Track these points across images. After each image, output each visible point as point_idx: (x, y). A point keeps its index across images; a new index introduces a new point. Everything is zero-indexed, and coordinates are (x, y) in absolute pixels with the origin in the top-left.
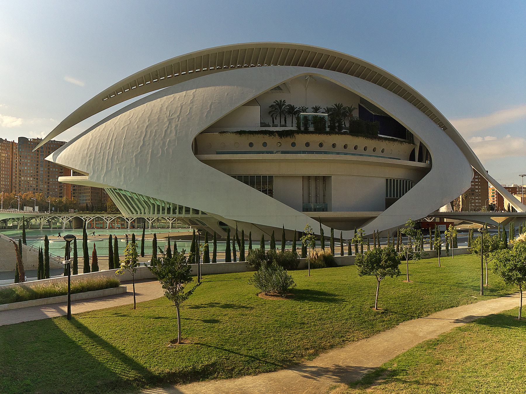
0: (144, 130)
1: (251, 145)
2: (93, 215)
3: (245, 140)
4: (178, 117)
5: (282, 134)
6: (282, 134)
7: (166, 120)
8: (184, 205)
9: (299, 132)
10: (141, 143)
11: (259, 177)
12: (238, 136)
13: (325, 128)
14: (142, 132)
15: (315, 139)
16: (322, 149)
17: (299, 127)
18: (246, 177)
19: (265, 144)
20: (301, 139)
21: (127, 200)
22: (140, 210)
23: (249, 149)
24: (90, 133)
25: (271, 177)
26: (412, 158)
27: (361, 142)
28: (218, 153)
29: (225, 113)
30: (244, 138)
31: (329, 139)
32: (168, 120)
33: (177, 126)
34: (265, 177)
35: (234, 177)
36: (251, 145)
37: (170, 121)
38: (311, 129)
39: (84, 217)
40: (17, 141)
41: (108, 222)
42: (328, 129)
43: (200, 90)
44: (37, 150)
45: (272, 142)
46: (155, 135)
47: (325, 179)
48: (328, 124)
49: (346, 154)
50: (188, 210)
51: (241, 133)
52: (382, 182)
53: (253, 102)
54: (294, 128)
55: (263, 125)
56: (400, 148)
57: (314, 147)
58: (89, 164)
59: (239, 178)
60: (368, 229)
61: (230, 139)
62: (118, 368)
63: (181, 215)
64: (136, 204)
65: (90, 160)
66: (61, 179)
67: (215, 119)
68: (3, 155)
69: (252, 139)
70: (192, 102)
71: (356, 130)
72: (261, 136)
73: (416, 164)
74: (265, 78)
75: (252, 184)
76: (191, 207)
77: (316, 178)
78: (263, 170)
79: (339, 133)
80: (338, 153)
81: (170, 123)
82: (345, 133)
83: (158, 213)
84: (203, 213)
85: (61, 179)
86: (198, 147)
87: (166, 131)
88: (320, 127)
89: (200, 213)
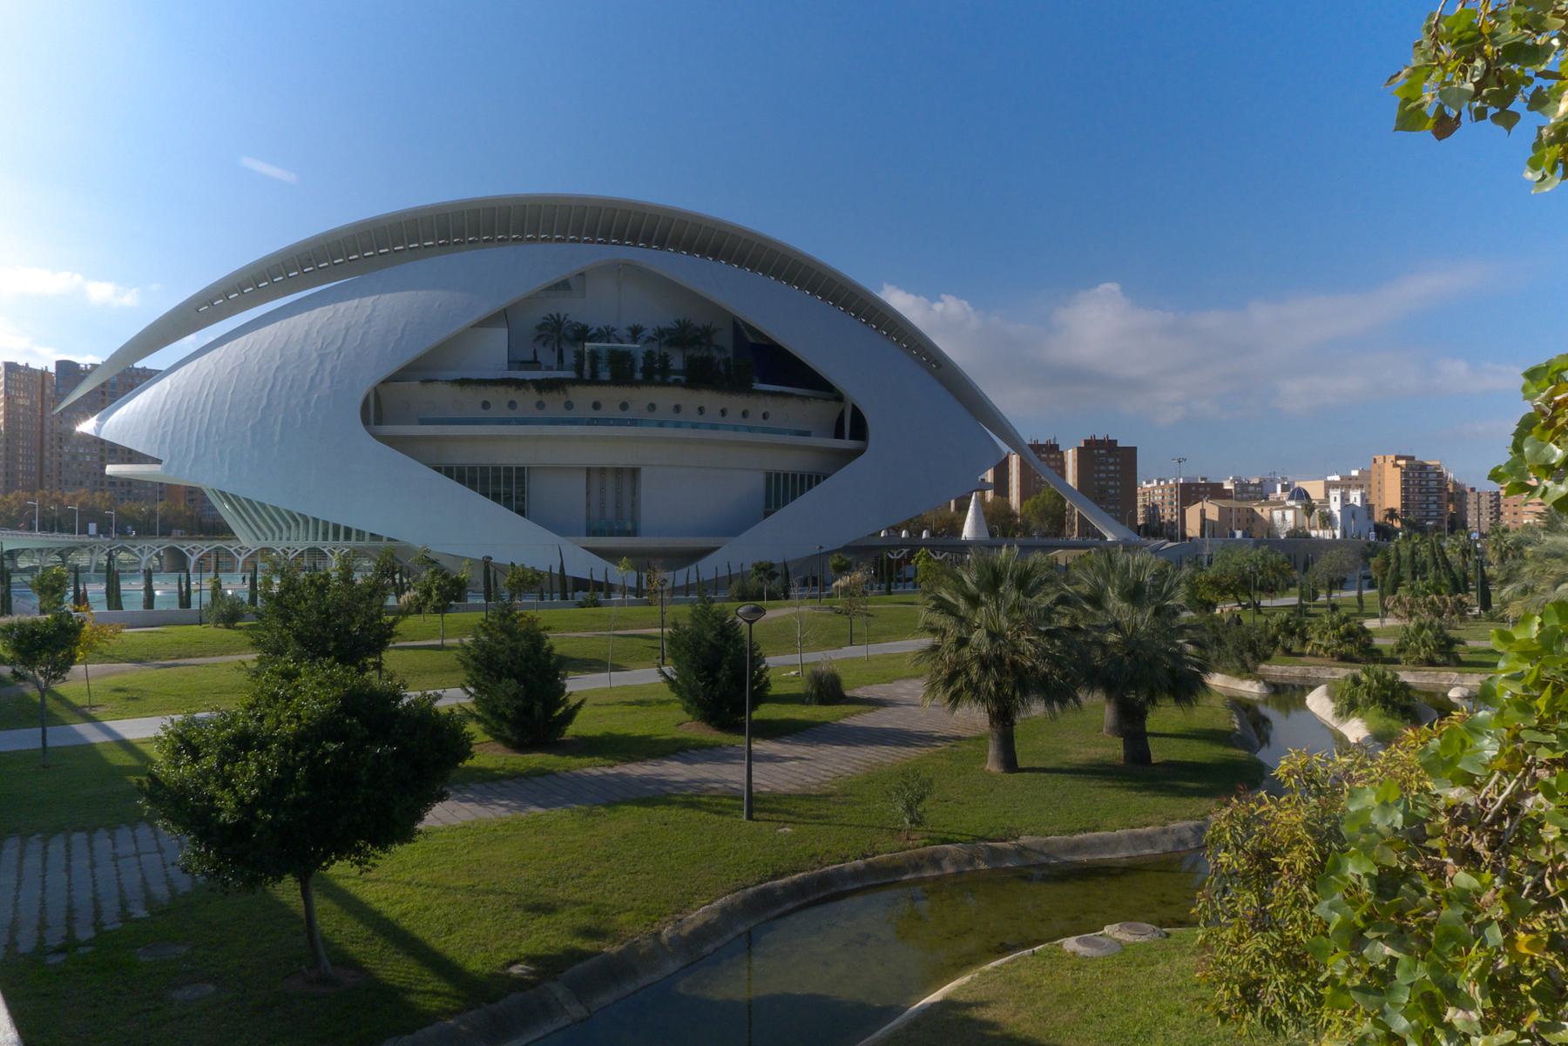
0: (270, 376)
1: (486, 405)
2: (207, 543)
3: (471, 399)
4: (339, 350)
5: (542, 386)
6: (542, 386)
7: (314, 355)
8: (343, 524)
9: (579, 381)
10: (264, 402)
11: (484, 469)
12: (457, 388)
13: (633, 371)
14: (265, 380)
15: (612, 396)
16: (628, 415)
17: (579, 368)
18: (461, 470)
19: (512, 405)
20: (583, 396)
21: (249, 508)
22: (281, 530)
23: (483, 414)
24: (183, 369)
25: (520, 470)
26: (839, 434)
27: (711, 400)
28: (423, 422)
29: (436, 338)
30: (469, 391)
31: (641, 397)
32: (320, 356)
33: (333, 369)
34: (508, 469)
35: (438, 469)
36: (486, 405)
37: (322, 358)
38: (605, 375)
39: (186, 546)
40: (52, 369)
41: (241, 559)
42: (639, 376)
43: (388, 296)
44: (61, 413)
45: (527, 400)
46: (291, 387)
47: (635, 472)
48: (640, 364)
49: (678, 425)
50: (360, 534)
51: (463, 382)
52: (758, 482)
53: (501, 317)
54: (570, 374)
55: (513, 363)
56: (816, 411)
57: (610, 410)
58: (163, 442)
59: (448, 472)
60: (707, 568)
61: (443, 396)
62: (395, 969)
63: (361, 544)
64: (265, 522)
65: (164, 434)
66: (110, 469)
67: (409, 356)
68: (21, 402)
69: (490, 394)
70: (368, 321)
71: (701, 376)
72: (501, 389)
73: (847, 444)
74: (520, 272)
75: (472, 484)
76: (354, 525)
77: (618, 471)
78: (507, 456)
79: (664, 383)
80: (661, 424)
81: (321, 363)
82: (677, 383)
83: (325, 538)
84: (390, 539)
85: (110, 469)
86: (377, 411)
87: (312, 379)
88: (622, 371)
89: (367, 537)
